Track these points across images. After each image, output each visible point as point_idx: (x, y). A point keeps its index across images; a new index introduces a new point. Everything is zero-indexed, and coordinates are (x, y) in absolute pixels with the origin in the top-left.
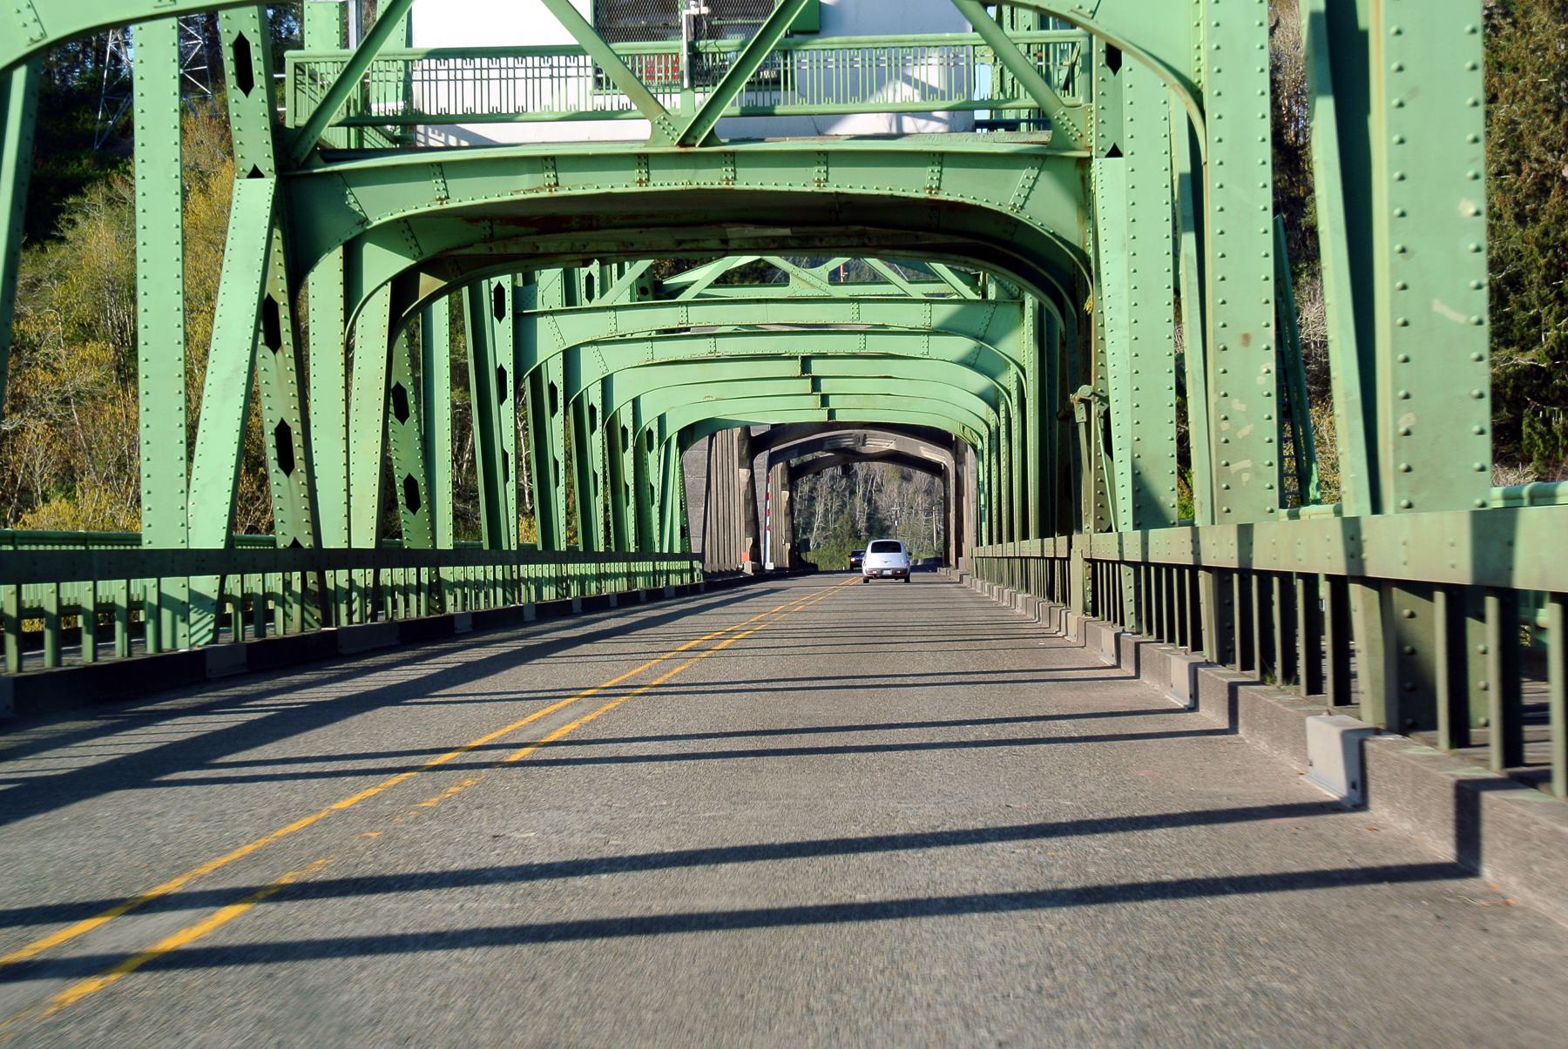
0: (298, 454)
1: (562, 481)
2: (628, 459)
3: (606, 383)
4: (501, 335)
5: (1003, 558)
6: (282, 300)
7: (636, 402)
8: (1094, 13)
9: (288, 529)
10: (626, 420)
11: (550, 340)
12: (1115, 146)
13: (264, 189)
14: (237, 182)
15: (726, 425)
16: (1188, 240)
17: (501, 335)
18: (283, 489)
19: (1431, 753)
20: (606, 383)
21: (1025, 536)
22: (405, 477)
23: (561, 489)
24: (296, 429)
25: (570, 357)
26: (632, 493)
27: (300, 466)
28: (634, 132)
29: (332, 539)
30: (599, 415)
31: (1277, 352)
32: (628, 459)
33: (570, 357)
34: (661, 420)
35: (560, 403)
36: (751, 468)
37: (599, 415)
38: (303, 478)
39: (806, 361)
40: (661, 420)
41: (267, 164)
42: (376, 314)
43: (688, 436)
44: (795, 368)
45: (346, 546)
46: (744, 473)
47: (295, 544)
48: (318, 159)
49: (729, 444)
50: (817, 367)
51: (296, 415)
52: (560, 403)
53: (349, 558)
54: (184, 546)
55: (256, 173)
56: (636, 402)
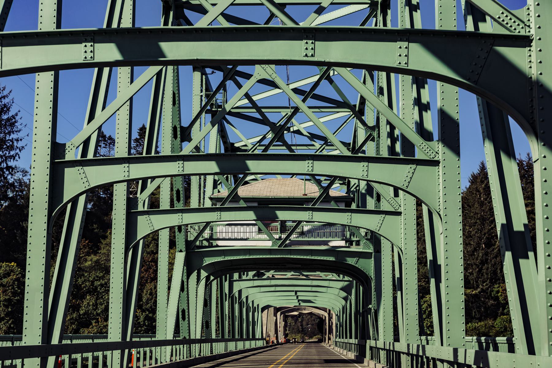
0: (187, 316)
1: (227, 320)
2: (251, 314)
3: (247, 297)
4: (226, 285)
5: (347, 343)
6: (185, 281)
7: (253, 302)
8: (379, 230)
9: (183, 334)
10: (251, 305)
11: (237, 286)
12: (378, 250)
13: (183, 254)
14: (177, 253)
15: (271, 306)
16: (397, 275)
17: (226, 285)
18: (183, 325)
19: (380, 11)
20: (247, 297)
21: (351, 338)
22: (206, 321)
23: (227, 322)
24: (186, 311)
25: (240, 292)
26: (251, 323)
27: (187, 319)
28: (268, 244)
29: (192, 337)
30: (245, 304)
31: (418, 305)
32: (251, 314)
33: (240, 292)
34: (258, 305)
35: (227, 298)
36: (276, 317)
37: (245, 304)
38: (187, 322)
39: (296, 292)
40: (258, 305)
41: (184, 249)
42: (203, 283)
43: (263, 309)
44: (294, 293)
45: (195, 338)
46: (275, 318)
47: (185, 338)
48: (196, 248)
49: (272, 310)
50: (299, 294)
51: (187, 308)
52: (227, 298)
53: (195, 341)
54: (165, 339)
55: (181, 251)
56: (253, 302)
